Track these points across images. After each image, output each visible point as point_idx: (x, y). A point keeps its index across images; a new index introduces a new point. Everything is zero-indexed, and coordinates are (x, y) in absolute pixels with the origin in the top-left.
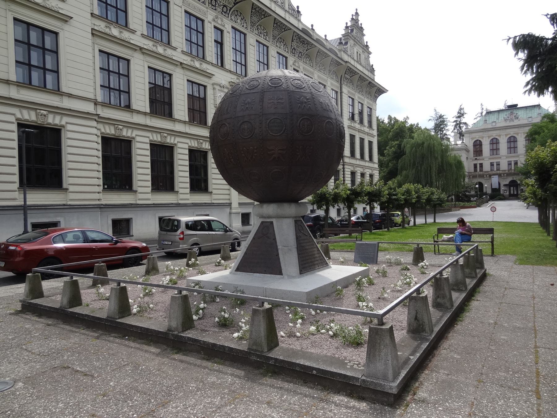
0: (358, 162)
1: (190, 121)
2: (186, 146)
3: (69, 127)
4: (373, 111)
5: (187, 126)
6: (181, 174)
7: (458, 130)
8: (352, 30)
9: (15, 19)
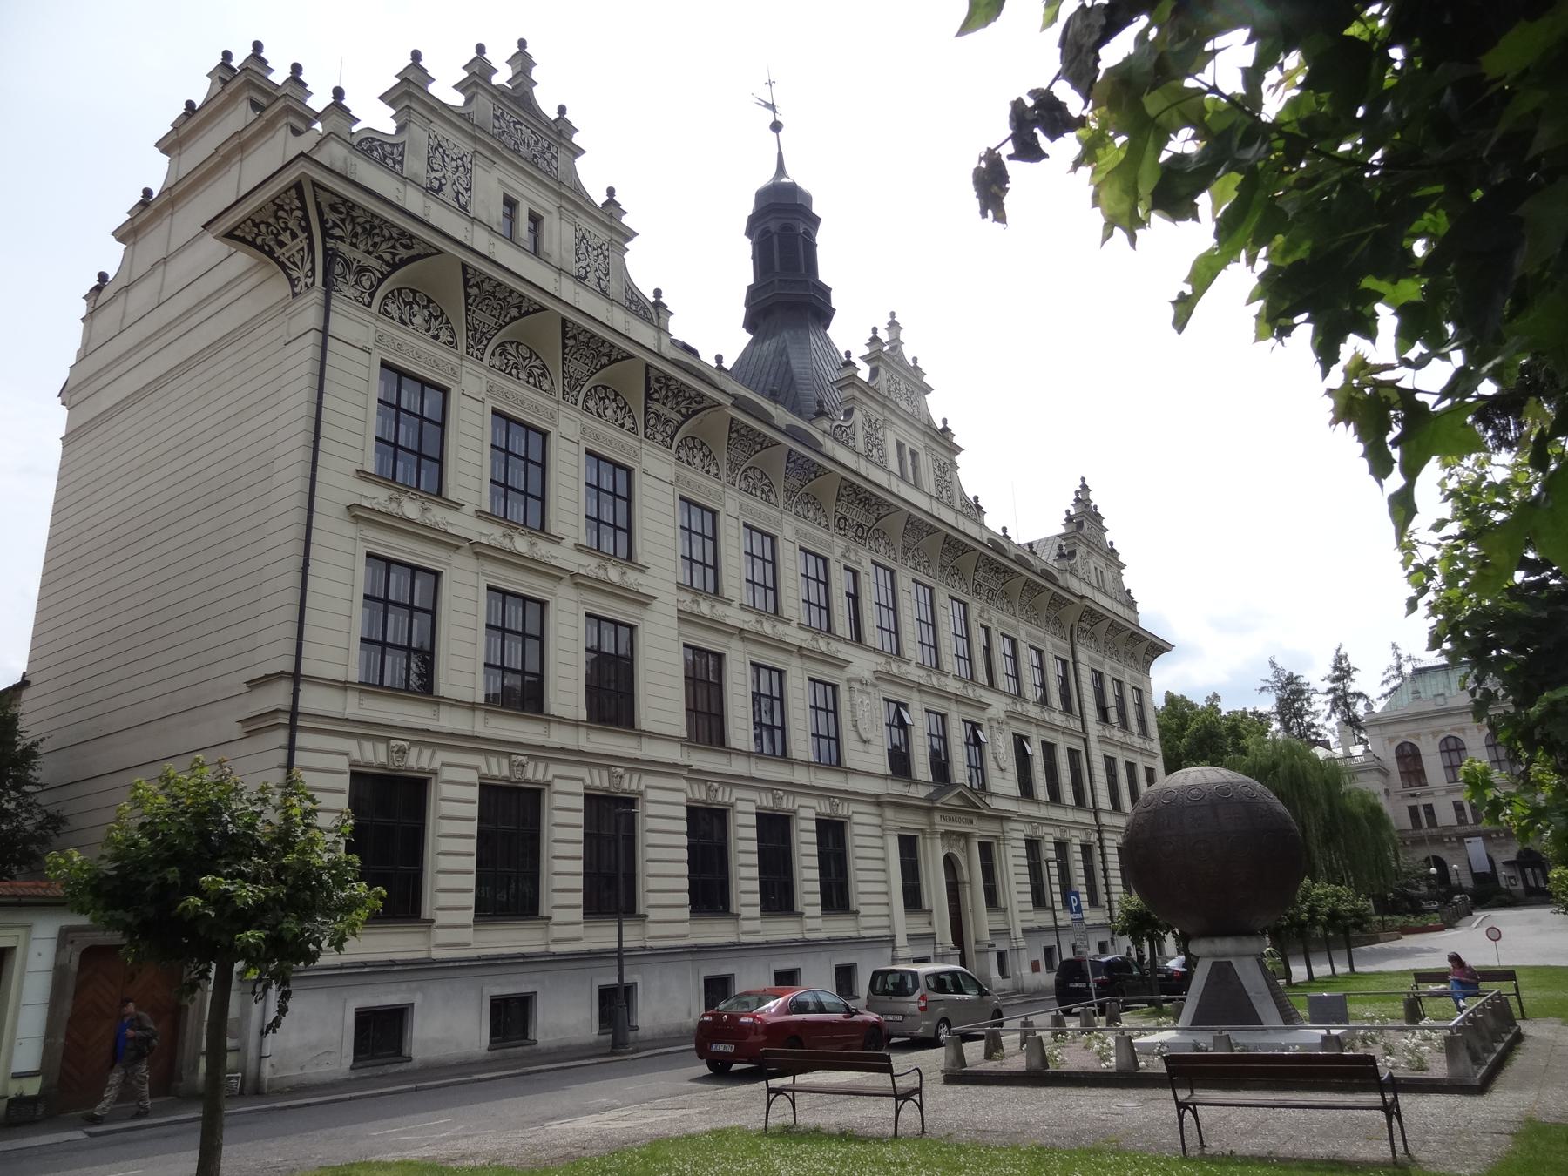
0: (1044, 812)
1: (690, 738)
2: (579, 788)
3: (651, 794)
4: (1145, 695)
5: (480, 715)
6: (560, 865)
7: (1342, 713)
8: (1080, 525)
9: (369, 555)
